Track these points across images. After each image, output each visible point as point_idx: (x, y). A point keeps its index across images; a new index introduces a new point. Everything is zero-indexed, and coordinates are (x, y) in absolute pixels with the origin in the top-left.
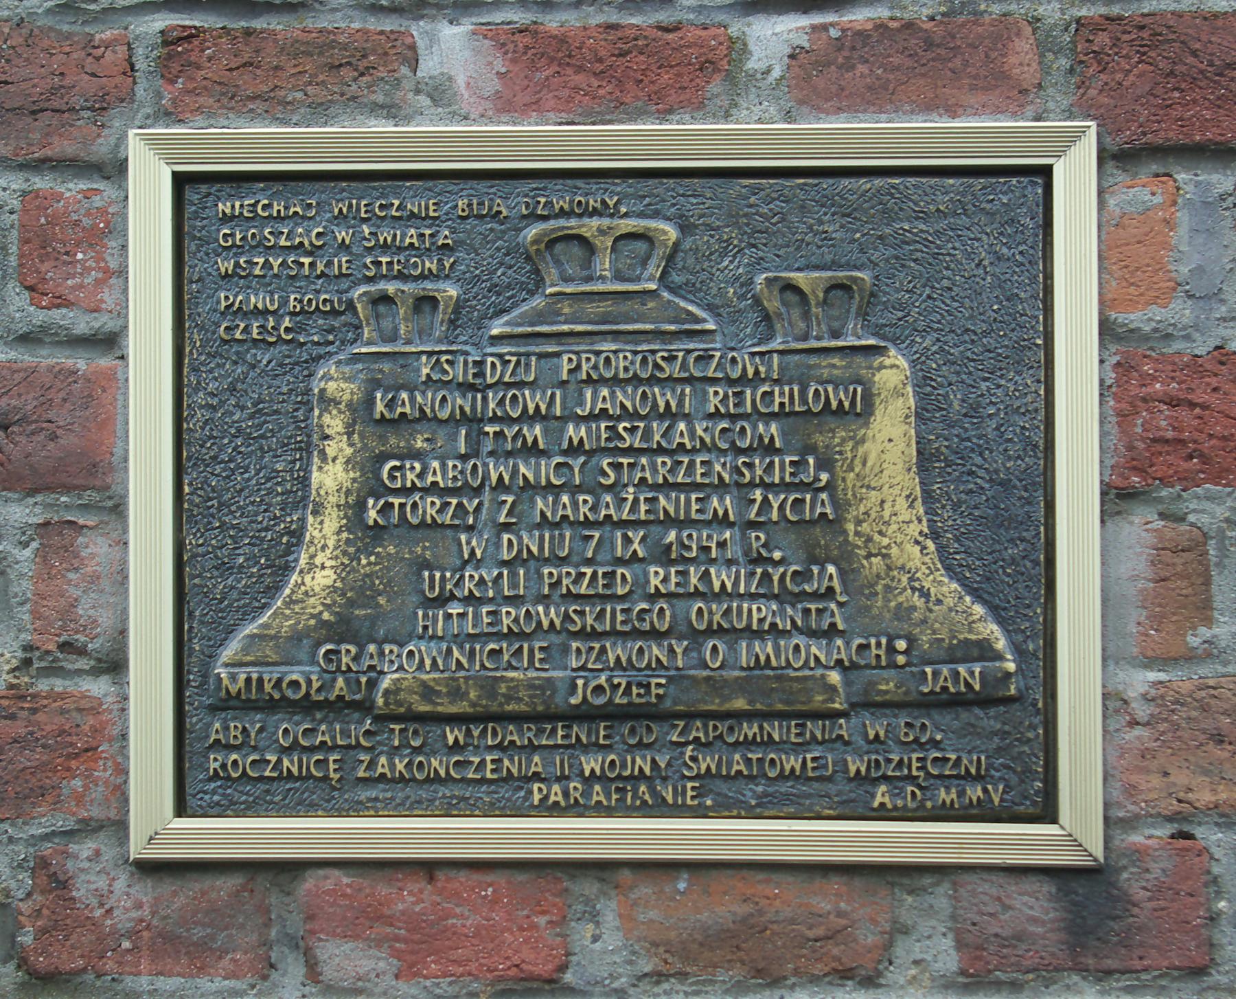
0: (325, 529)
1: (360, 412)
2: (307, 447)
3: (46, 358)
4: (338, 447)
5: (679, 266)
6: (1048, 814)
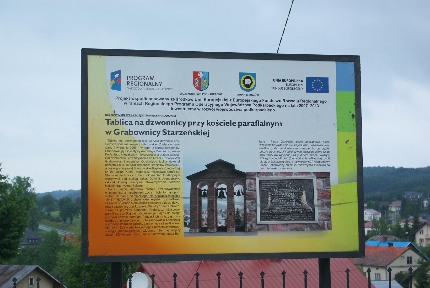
0: (269, 202)
1: (271, 195)
2: (268, 197)
3: (251, 192)
4: (270, 197)
5: (18, 206)
6: (315, 220)
